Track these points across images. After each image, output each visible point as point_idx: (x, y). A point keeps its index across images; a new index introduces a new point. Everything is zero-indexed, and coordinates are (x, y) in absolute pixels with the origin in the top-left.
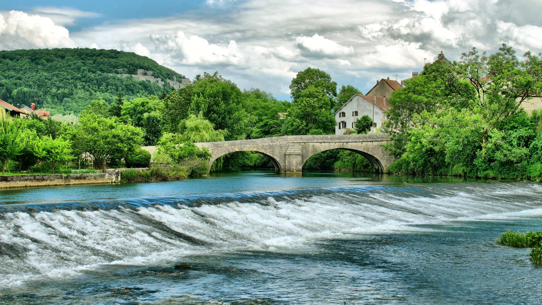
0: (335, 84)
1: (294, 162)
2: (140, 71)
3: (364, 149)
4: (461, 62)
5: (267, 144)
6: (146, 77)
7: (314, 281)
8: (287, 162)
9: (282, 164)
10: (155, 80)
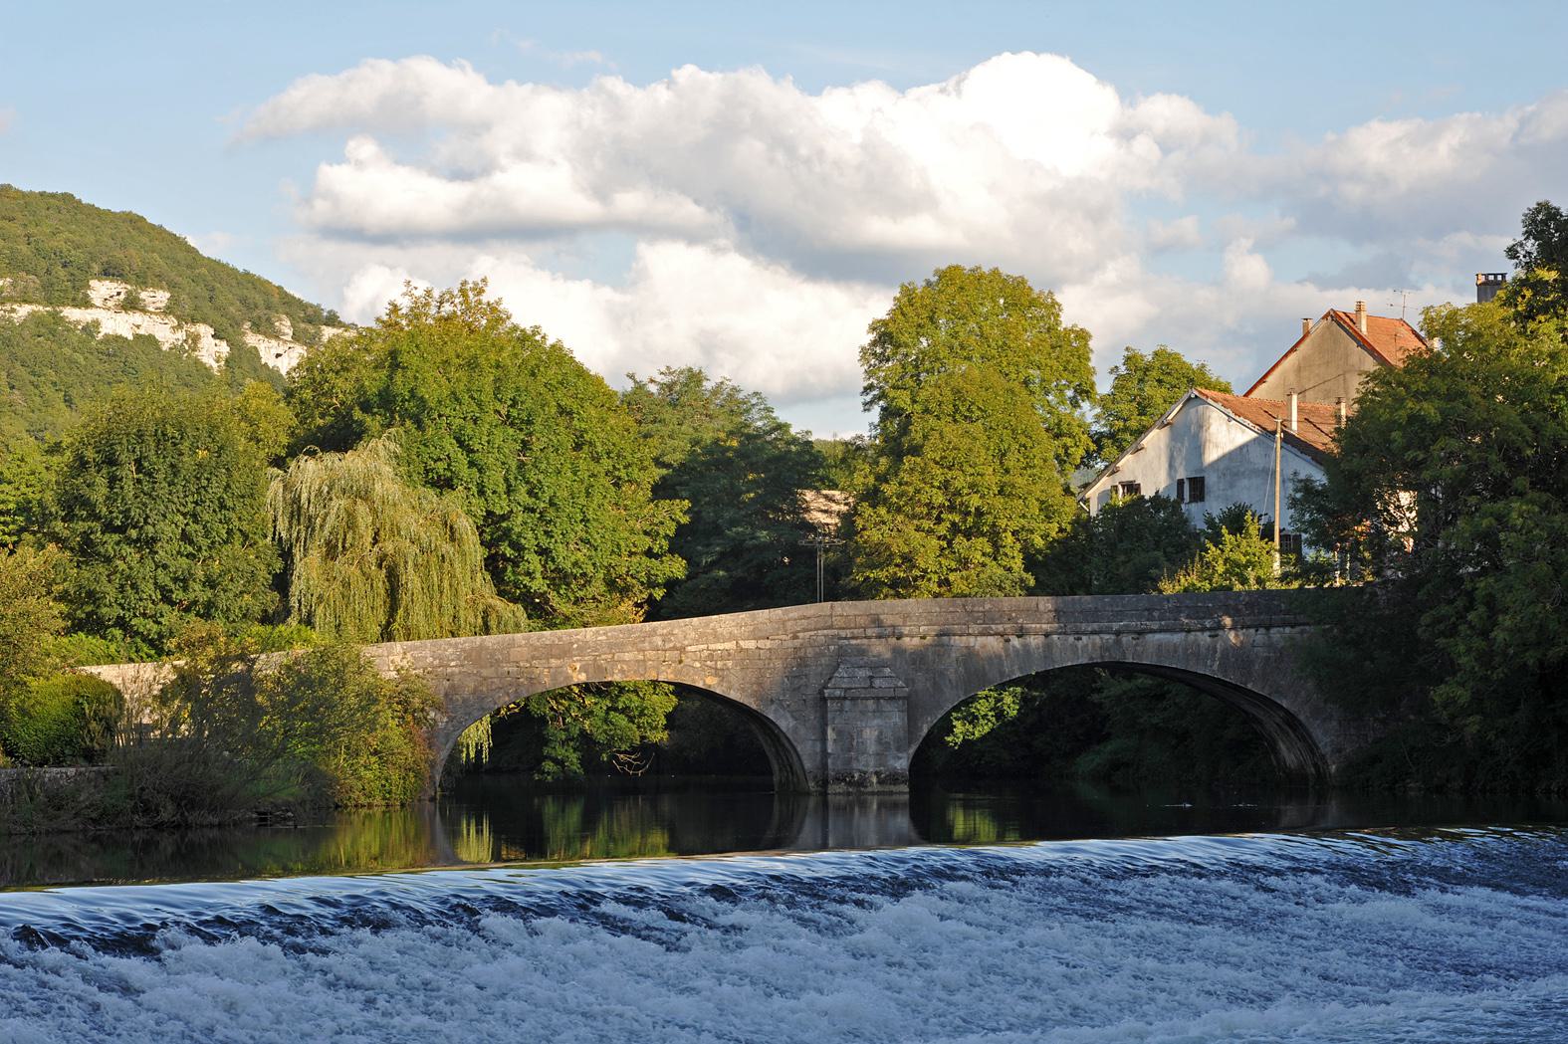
0: (1083, 336)
1: (870, 735)
2: (101, 289)
3: (1223, 666)
4: (953, 932)
5: (730, 645)
6: (137, 317)
7: (1190, 954)
8: (831, 735)
9: (807, 752)
10: (181, 335)
